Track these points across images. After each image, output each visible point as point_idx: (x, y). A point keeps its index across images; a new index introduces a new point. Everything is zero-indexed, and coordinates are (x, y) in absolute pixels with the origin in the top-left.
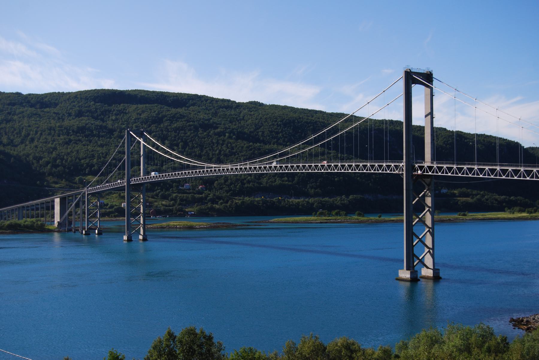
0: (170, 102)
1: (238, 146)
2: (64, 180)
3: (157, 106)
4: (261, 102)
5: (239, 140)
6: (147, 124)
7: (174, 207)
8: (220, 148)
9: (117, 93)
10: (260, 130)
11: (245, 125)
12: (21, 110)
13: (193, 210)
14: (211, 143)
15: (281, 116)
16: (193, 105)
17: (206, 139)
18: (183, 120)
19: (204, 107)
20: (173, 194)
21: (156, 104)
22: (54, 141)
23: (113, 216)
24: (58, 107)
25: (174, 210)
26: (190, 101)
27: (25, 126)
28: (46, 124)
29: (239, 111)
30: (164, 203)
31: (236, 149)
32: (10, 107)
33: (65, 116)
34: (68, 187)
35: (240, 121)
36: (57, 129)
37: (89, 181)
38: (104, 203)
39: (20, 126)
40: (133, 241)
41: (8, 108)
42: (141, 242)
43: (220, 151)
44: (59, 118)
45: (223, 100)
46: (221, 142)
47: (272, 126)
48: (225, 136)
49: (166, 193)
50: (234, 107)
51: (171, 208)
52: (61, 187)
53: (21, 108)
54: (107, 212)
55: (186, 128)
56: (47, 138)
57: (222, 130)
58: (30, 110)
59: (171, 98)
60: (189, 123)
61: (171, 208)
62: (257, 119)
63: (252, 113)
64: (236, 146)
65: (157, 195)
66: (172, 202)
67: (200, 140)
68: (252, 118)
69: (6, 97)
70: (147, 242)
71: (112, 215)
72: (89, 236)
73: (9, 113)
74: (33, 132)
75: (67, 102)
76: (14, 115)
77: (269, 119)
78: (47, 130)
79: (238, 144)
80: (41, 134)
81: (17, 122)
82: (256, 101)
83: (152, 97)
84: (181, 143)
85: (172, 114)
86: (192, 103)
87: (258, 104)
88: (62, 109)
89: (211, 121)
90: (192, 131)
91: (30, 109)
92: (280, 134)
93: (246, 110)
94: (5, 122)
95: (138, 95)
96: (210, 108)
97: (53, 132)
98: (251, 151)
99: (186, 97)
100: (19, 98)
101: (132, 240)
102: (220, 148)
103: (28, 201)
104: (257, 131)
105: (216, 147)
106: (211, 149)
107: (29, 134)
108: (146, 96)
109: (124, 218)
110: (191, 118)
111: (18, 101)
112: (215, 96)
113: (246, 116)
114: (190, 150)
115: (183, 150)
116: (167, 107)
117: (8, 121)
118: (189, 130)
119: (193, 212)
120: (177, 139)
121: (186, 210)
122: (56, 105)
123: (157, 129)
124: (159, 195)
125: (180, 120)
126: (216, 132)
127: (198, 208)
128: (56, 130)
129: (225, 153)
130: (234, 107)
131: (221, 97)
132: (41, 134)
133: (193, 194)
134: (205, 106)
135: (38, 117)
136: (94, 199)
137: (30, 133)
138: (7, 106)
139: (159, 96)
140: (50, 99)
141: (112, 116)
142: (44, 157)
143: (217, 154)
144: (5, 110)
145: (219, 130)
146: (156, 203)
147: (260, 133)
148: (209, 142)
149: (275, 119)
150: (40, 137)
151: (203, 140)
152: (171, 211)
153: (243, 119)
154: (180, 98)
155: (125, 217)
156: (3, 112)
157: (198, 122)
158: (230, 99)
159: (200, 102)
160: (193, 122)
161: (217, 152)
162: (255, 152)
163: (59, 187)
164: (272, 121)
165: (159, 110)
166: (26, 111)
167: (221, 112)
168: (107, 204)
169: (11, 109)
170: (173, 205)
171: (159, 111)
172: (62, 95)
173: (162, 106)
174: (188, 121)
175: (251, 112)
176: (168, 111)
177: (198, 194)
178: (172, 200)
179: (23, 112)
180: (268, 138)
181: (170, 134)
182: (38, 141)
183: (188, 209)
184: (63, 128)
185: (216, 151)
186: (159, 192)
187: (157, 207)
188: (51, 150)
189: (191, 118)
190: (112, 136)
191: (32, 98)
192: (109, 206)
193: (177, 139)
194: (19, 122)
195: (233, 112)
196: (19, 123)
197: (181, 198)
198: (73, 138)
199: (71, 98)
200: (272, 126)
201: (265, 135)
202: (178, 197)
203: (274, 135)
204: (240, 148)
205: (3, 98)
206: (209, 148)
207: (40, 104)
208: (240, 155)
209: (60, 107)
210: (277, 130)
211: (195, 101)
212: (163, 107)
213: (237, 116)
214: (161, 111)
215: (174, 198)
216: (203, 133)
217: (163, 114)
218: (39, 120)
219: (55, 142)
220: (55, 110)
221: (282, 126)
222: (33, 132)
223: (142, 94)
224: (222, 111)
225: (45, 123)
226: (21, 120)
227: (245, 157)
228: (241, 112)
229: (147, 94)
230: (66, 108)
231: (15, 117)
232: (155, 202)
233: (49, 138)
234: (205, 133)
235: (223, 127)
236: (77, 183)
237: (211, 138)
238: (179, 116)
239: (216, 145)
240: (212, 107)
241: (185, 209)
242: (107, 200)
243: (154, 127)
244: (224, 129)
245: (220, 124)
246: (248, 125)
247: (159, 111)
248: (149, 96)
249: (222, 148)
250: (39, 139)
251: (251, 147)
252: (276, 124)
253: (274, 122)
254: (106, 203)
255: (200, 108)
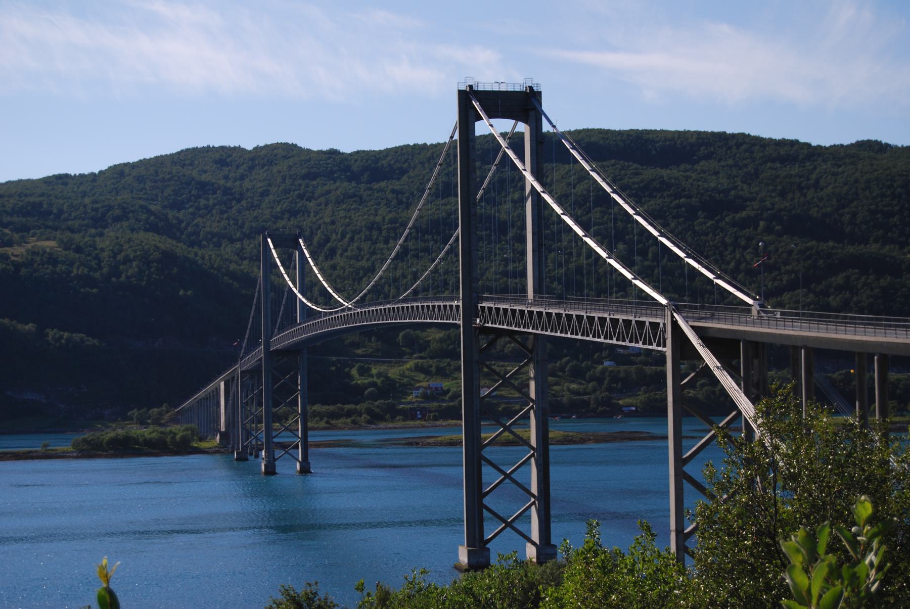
0: (654, 152)
1: (780, 250)
2: (373, 338)
3: (614, 165)
4: (883, 142)
5: (785, 236)
6: (585, 206)
7: (593, 396)
8: (738, 256)
9: (554, 139)
10: (846, 210)
11: (815, 200)
12: (327, 188)
13: (634, 402)
14: (719, 244)
15: (905, 173)
16: (708, 157)
17: (711, 235)
18: (666, 193)
19: (730, 162)
20: (596, 366)
21: (613, 161)
22: (374, 253)
23: (432, 418)
24: (405, 178)
25: (592, 402)
26: (702, 148)
27: (324, 223)
28: (365, 217)
29: (811, 167)
30: (574, 386)
31: (776, 258)
32: (307, 181)
33: (415, 196)
34: (380, 354)
35: (805, 191)
36: (386, 226)
37: (427, 339)
38: (442, 388)
39: (314, 223)
40: (277, 473)
41: (300, 185)
42: (263, 475)
43: (738, 263)
44: (400, 202)
45: (783, 143)
46: (743, 243)
47: (880, 199)
48: (756, 228)
49: (583, 365)
50: (801, 157)
51: (586, 397)
52: (364, 353)
53: (325, 185)
54: (442, 408)
55: (668, 213)
56: (362, 246)
57: (752, 214)
58: (344, 186)
59: (658, 145)
60: (677, 201)
61: (586, 397)
62: (846, 184)
63: (840, 169)
64: (777, 250)
65: (562, 369)
66: (591, 383)
67: (696, 238)
68: (836, 181)
69: (301, 161)
70: (309, 477)
71: (430, 416)
72: (246, 462)
73: (301, 197)
74: (337, 235)
75: (426, 165)
76: (309, 200)
77: (875, 182)
78: (364, 229)
79: (783, 244)
80: (352, 239)
81: (312, 214)
82: (873, 138)
83: (614, 143)
84: (651, 249)
85: (642, 181)
86: (706, 152)
87: (877, 147)
88: (412, 182)
89: (732, 193)
90: (682, 219)
91: (345, 184)
92: (896, 218)
93: (829, 163)
94: (287, 215)
95: (582, 142)
96: (745, 162)
97: (375, 233)
98: (809, 262)
99: (693, 140)
100: (328, 161)
101: (277, 471)
102: (739, 256)
103: (200, 390)
104: (840, 212)
105: (731, 254)
106: (719, 258)
107: (327, 240)
108: (601, 142)
109: (459, 422)
110: (685, 188)
111: (325, 169)
112: (765, 134)
113: (824, 177)
114: (672, 263)
115: (655, 263)
116: (639, 166)
117: (293, 213)
118: (674, 217)
119: (634, 407)
120: (644, 240)
121: (621, 402)
122: (403, 172)
123: (603, 217)
124: (566, 370)
125: (659, 194)
126: (736, 218)
127: (645, 398)
128: (382, 229)
129: (748, 266)
130: (801, 157)
131: (777, 136)
132: (352, 239)
133: (640, 366)
134: (734, 159)
135: (355, 201)
136: (426, 380)
137: (330, 237)
138: (300, 182)
139: (629, 142)
140: (392, 162)
141: (514, 192)
142: (343, 289)
143: (731, 269)
144: (294, 190)
145: (744, 214)
146: (556, 388)
147: (847, 218)
148: (716, 242)
149: (889, 183)
150: (349, 246)
151: (703, 238)
152: (586, 403)
153: (816, 185)
154: (679, 142)
155: (462, 419)
156: (289, 193)
157: (699, 196)
158: (796, 138)
159: (724, 149)
160: (689, 197)
161: (732, 264)
162: (818, 264)
163: (362, 353)
164: (881, 186)
165: (617, 173)
166: (336, 189)
167: (769, 171)
168: (449, 391)
169: (307, 186)
170: (594, 390)
171: (616, 176)
172: (418, 151)
173: (626, 164)
174: (677, 196)
175: (839, 166)
176: (637, 174)
177: (655, 366)
178: (592, 379)
179: (329, 192)
180: (864, 227)
181: (630, 229)
182: (341, 255)
183: (624, 401)
184: (398, 225)
185: (728, 263)
186: (567, 363)
187: (554, 396)
188: (361, 272)
189: (685, 188)
190: (501, 236)
191: (356, 161)
192: (450, 394)
193: (644, 240)
194: (316, 213)
195: (796, 170)
196: (315, 216)
197: (612, 374)
198: (414, 245)
199: (435, 156)
200: (880, 199)
201: (858, 222)
202: (607, 374)
203: (880, 220)
204: (785, 255)
205: (296, 164)
206: (714, 257)
207: (368, 173)
208: (783, 271)
209: (409, 177)
210: (890, 208)
211: (712, 149)
212: (629, 166)
213: (802, 179)
214: (619, 175)
215: (597, 374)
216: (705, 223)
217: (622, 182)
218: (355, 209)
219: (375, 256)
220: (396, 185)
221: (904, 196)
222: (337, 235)
223: (593, 139)
224: (771, 168)
225: (365, 214)
226: (321, 209)
227: (793, 274)
228: (815, 168)
229: (603, 138)
230: (419, 180)
231: (311, 205)
232: (557, 384)
233: (366, 246)
234: (710, 223)
235: (756, 207)
236: (401, 344)
237: (721, 234)
238: (658, 186)
239: (730, 249)
240: (748, 160)
241: (619, 400)
242: (454, 382)
243: (598, 214)
244: (759, 212)
245: (754, 199)
246: (821, 200)
247: (616, 176)
248: (608, 141)
249: (743, 255)
250: (346, 250)
251: (810, 252)
252: (889, 192)
253: (884, 190)
254: (445, 389)
255: (723, 163)
